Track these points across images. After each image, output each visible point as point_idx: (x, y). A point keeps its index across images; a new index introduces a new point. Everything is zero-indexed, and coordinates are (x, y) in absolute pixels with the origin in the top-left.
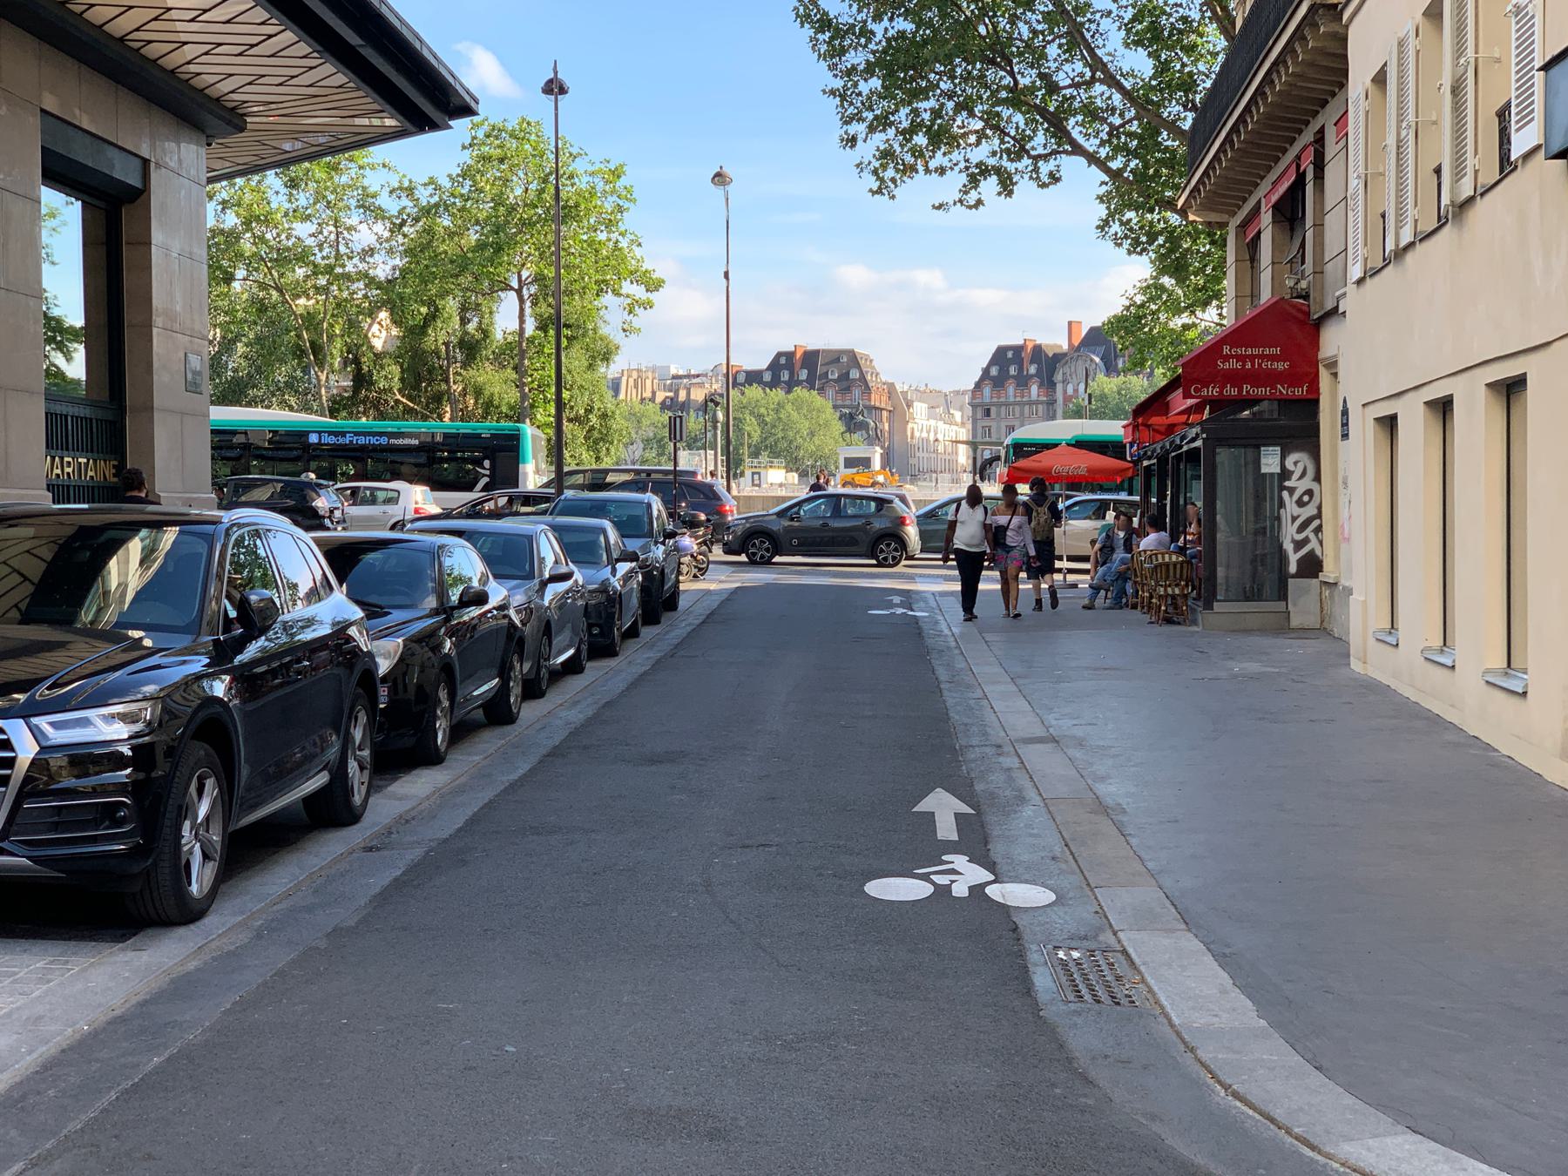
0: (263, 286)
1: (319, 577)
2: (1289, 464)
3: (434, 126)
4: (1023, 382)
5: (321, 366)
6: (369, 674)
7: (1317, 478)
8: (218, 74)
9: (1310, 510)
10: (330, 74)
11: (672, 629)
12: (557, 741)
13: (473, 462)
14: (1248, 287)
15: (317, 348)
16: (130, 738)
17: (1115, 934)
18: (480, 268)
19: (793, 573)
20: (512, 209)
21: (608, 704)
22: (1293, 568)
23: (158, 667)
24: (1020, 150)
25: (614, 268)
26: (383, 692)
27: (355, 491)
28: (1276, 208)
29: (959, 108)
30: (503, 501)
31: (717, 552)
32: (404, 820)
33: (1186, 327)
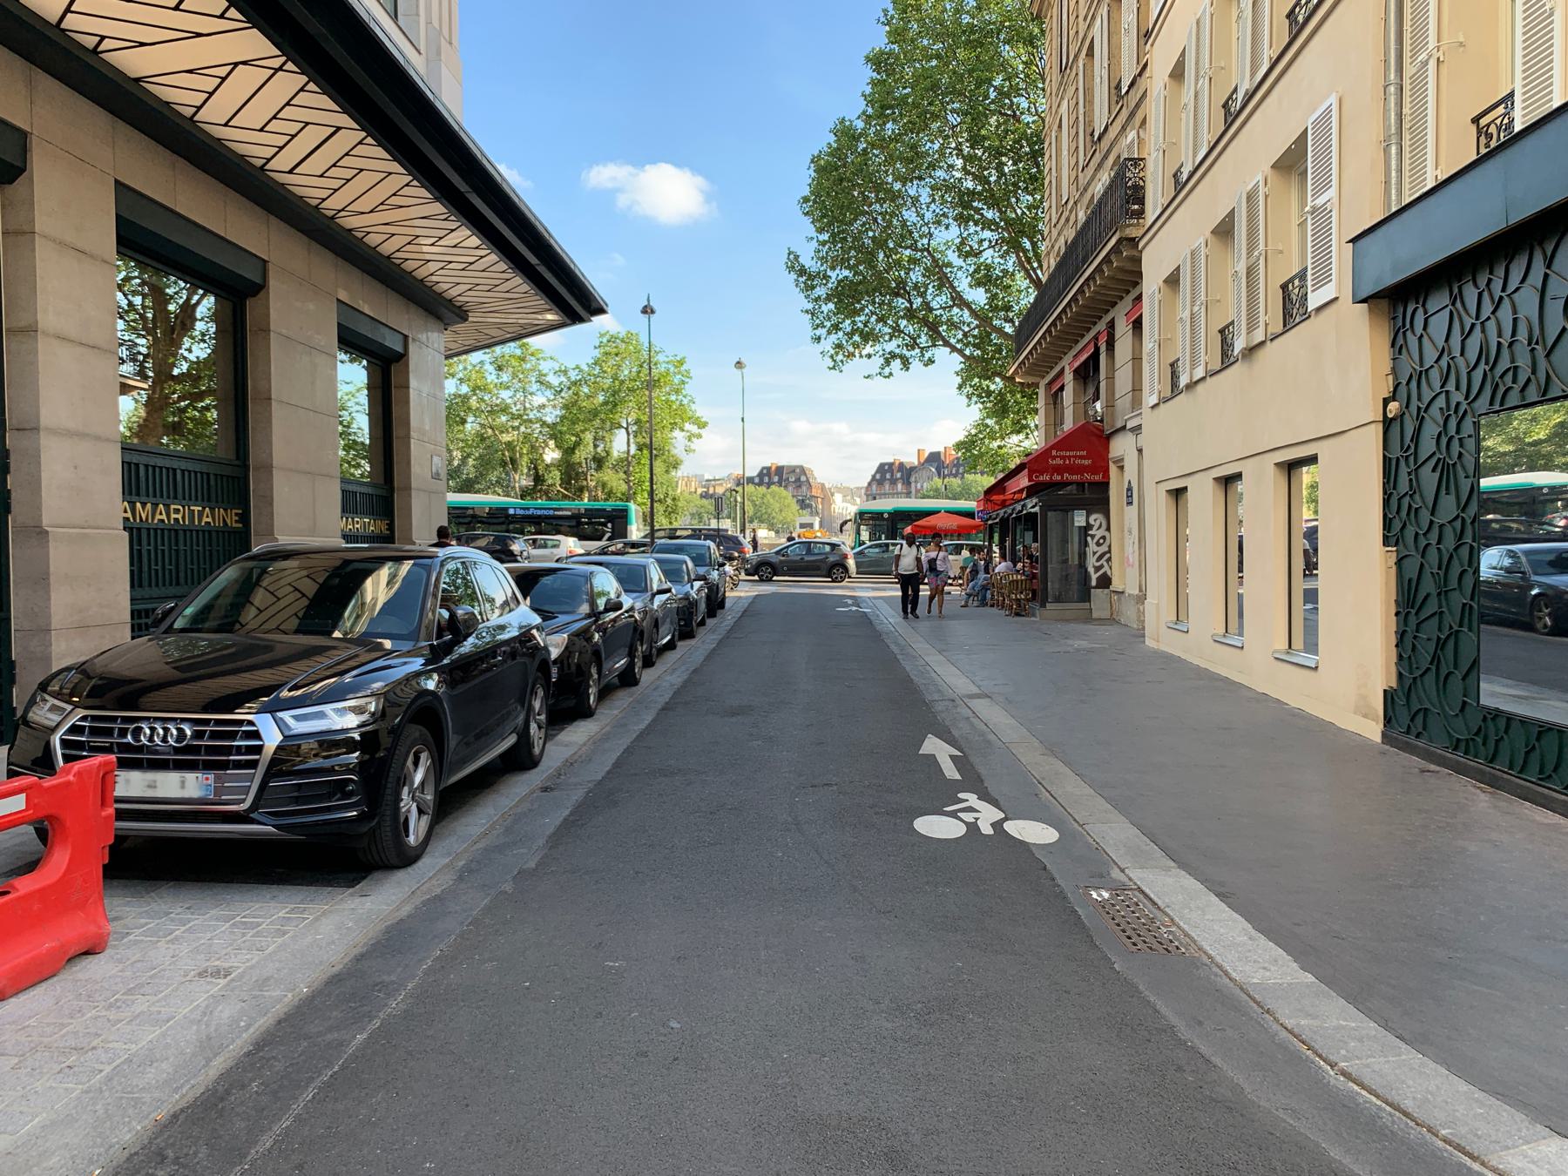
0: (483, 426)
1: (510, 594)
2: (1091, 521)
3: (581, 320)
4: (893, 482)
5: (515, 470)
6: (545, 665)
7: (1108, 529)
8: (449, 283)
9: (1104, 548)
10: (519, 283)
11: (727, 618)
12: (667, 698)
13: (603, 524)
14: (1055, 418)
15: (513, 461)
16: (359, 727)
17: (1123, 871)
18: (605, 416)
19: (782, 586)
20: (622, 382)
21: (695, 671)
22: (1094, 583)
23: (389, 667)
24: (913, 345)
25: (680, 416)
26: (554, 670)
27: (535, 541)
28: (1076, 372)
29: (878, 321)
30: (620, 546)
31: (743, 576)
32: (569, 764)
33: (1000, 447)
